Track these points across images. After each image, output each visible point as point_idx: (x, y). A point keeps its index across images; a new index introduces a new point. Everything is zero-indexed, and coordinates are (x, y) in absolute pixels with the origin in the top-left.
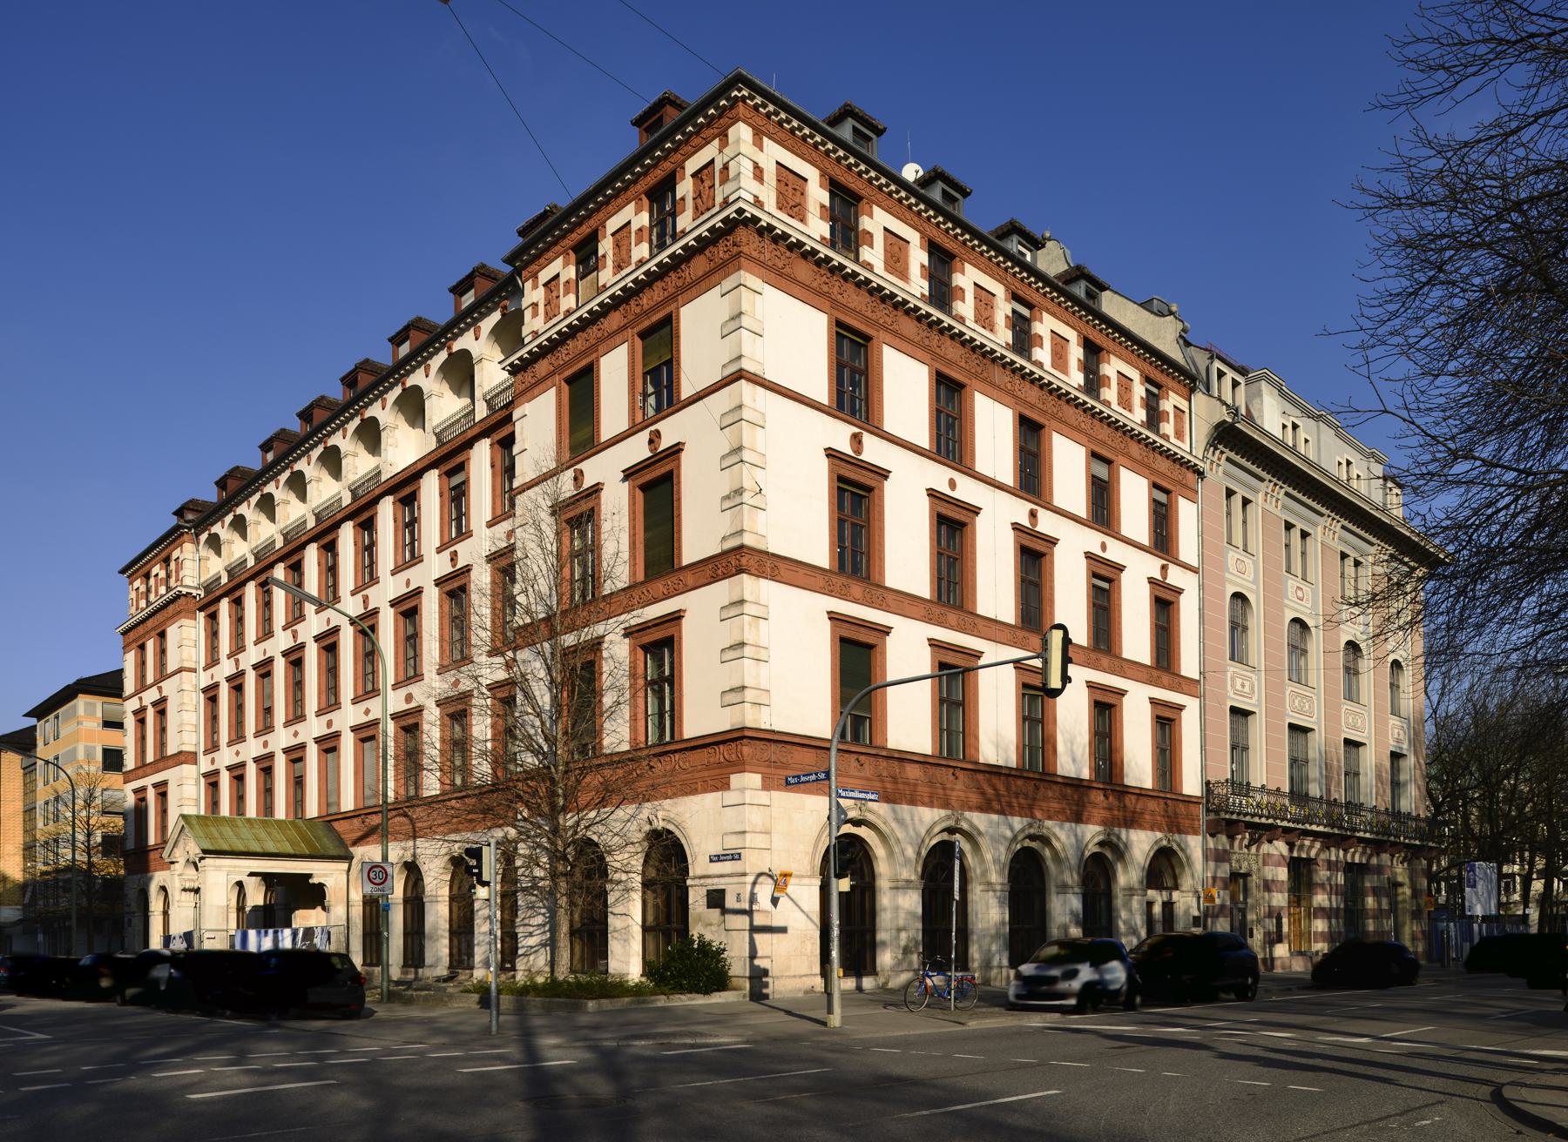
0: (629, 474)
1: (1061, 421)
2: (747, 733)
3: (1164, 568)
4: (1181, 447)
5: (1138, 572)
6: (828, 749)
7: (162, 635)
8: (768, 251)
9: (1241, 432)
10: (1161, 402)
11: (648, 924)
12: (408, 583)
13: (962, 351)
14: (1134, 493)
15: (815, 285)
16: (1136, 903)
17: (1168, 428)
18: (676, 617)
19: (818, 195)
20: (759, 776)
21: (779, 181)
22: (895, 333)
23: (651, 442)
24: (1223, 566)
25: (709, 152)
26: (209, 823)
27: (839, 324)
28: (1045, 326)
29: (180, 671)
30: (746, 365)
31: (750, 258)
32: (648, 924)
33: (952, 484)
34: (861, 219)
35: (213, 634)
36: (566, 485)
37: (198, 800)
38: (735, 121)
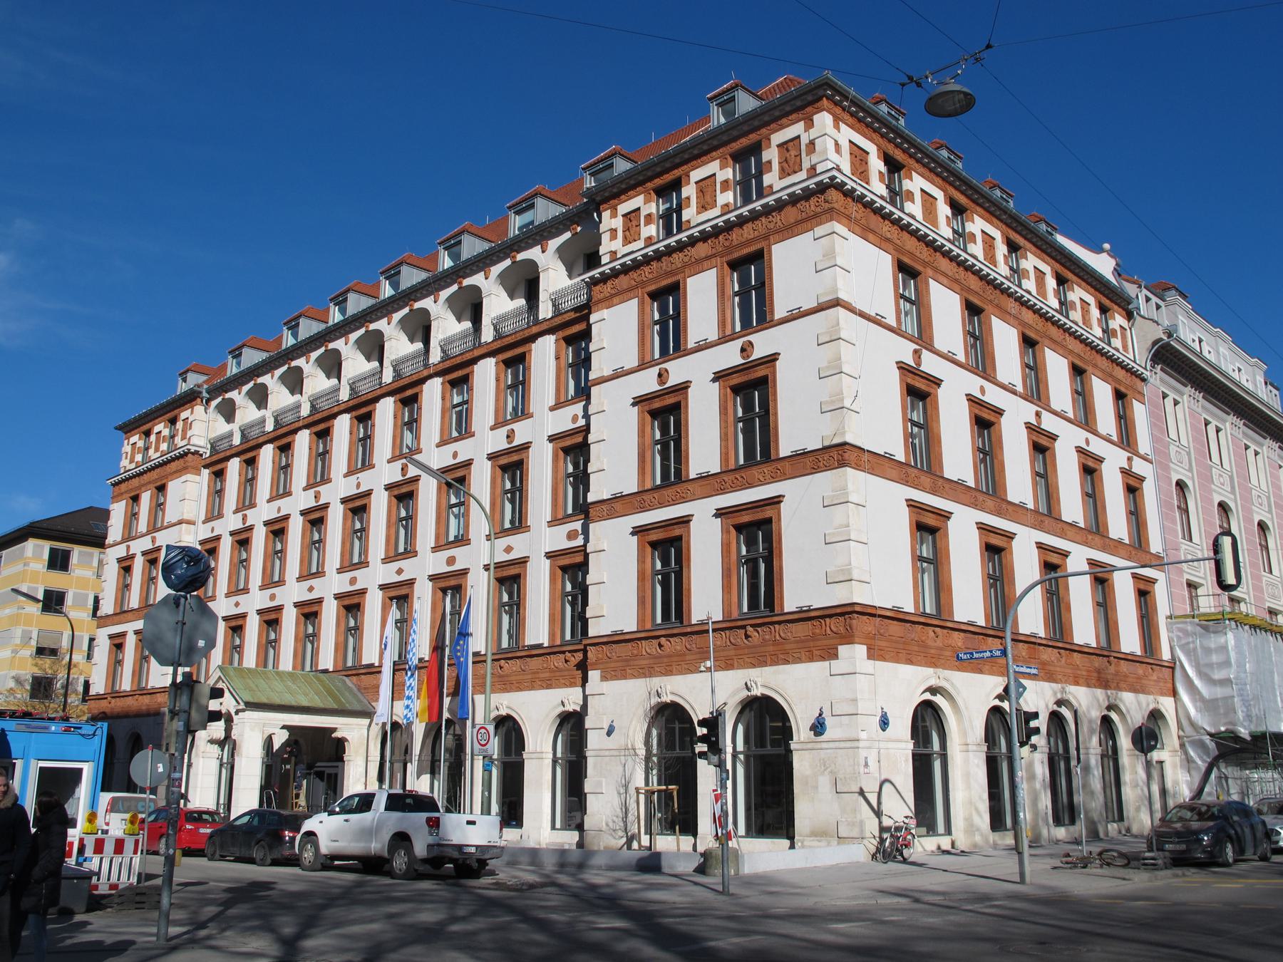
0: (719, 377)
3: (1129, 459)
5: (1113, 460)
7: (161, 489)
8: (855, 209)
9: (1173, 348)
12: (455, 455)
13: (980, 283)
14: (1102, 392)
18: (776, 501)
19: (876, 164)
20: (865, 647)
21: (851, 154)
23: (743, 350)
25: (796, 129)
29: (180, 522)
35: (217, 494)
36: (647, 382)
38: (820, 110)
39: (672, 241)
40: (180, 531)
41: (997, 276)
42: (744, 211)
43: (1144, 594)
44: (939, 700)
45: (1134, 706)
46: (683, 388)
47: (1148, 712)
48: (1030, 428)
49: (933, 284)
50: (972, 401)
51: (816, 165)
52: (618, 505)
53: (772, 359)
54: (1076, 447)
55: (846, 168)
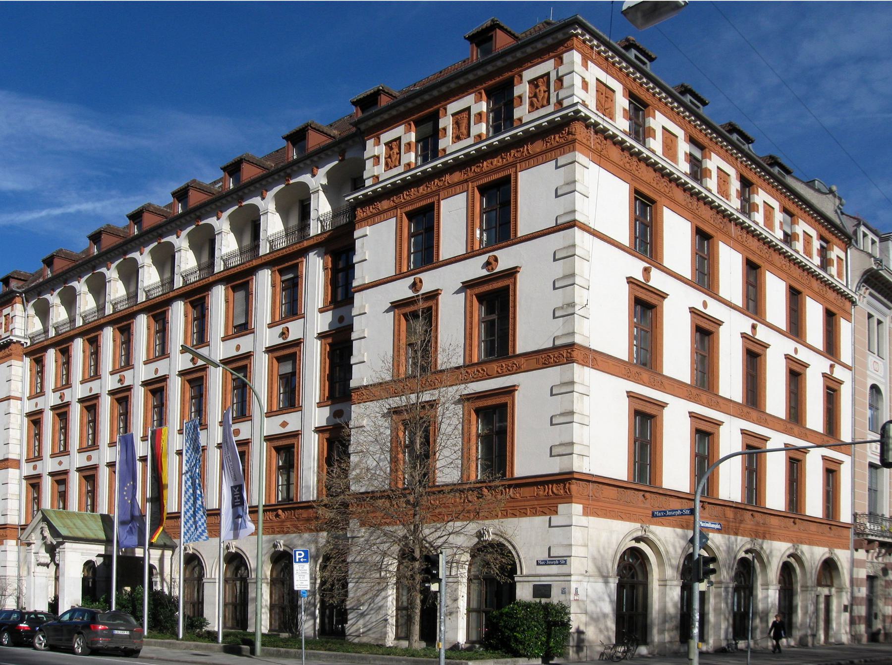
0: (467, 286)
1: (772, 264)
2: (576, 476)
3: (832, 366)
4: (840, 284)
6: (694, 500)
8: (593, 139)
9: (881, 276)
10: (828, 252)
11: (471, 607)
12: (238, 348)
14: (814, 313)
15: (621, 163)
16: (811, 595)
17: (834, 270)
19: (622, 102)
20: (581, 506)
21: (597, 91)
22: (672, 200)
24: (865, 366)
25: (547, 66)
26: (64, 516)
27: (637, 192)
28: (714, 162)
30: (579, 217)
31: (582, 143)
32: (471, 607)
33: (705, 305)
34: (647, 120)
36: (402, 290)
37: (20, 495)
39: (428, 167)
40: (9, 405)
41: (773, 239)
42: (495, 141)
43: (831, 473)
44: (642, 546)
45: (814, 554)
46: (434, 295)
47: (821, 562)
48: (693, 312)
49: (768, 274)
50: (693, 312)
51: (563, 99)
52: (371, 392)
53: (512, 273)
54: (690, 308)
55: (592, 103)
